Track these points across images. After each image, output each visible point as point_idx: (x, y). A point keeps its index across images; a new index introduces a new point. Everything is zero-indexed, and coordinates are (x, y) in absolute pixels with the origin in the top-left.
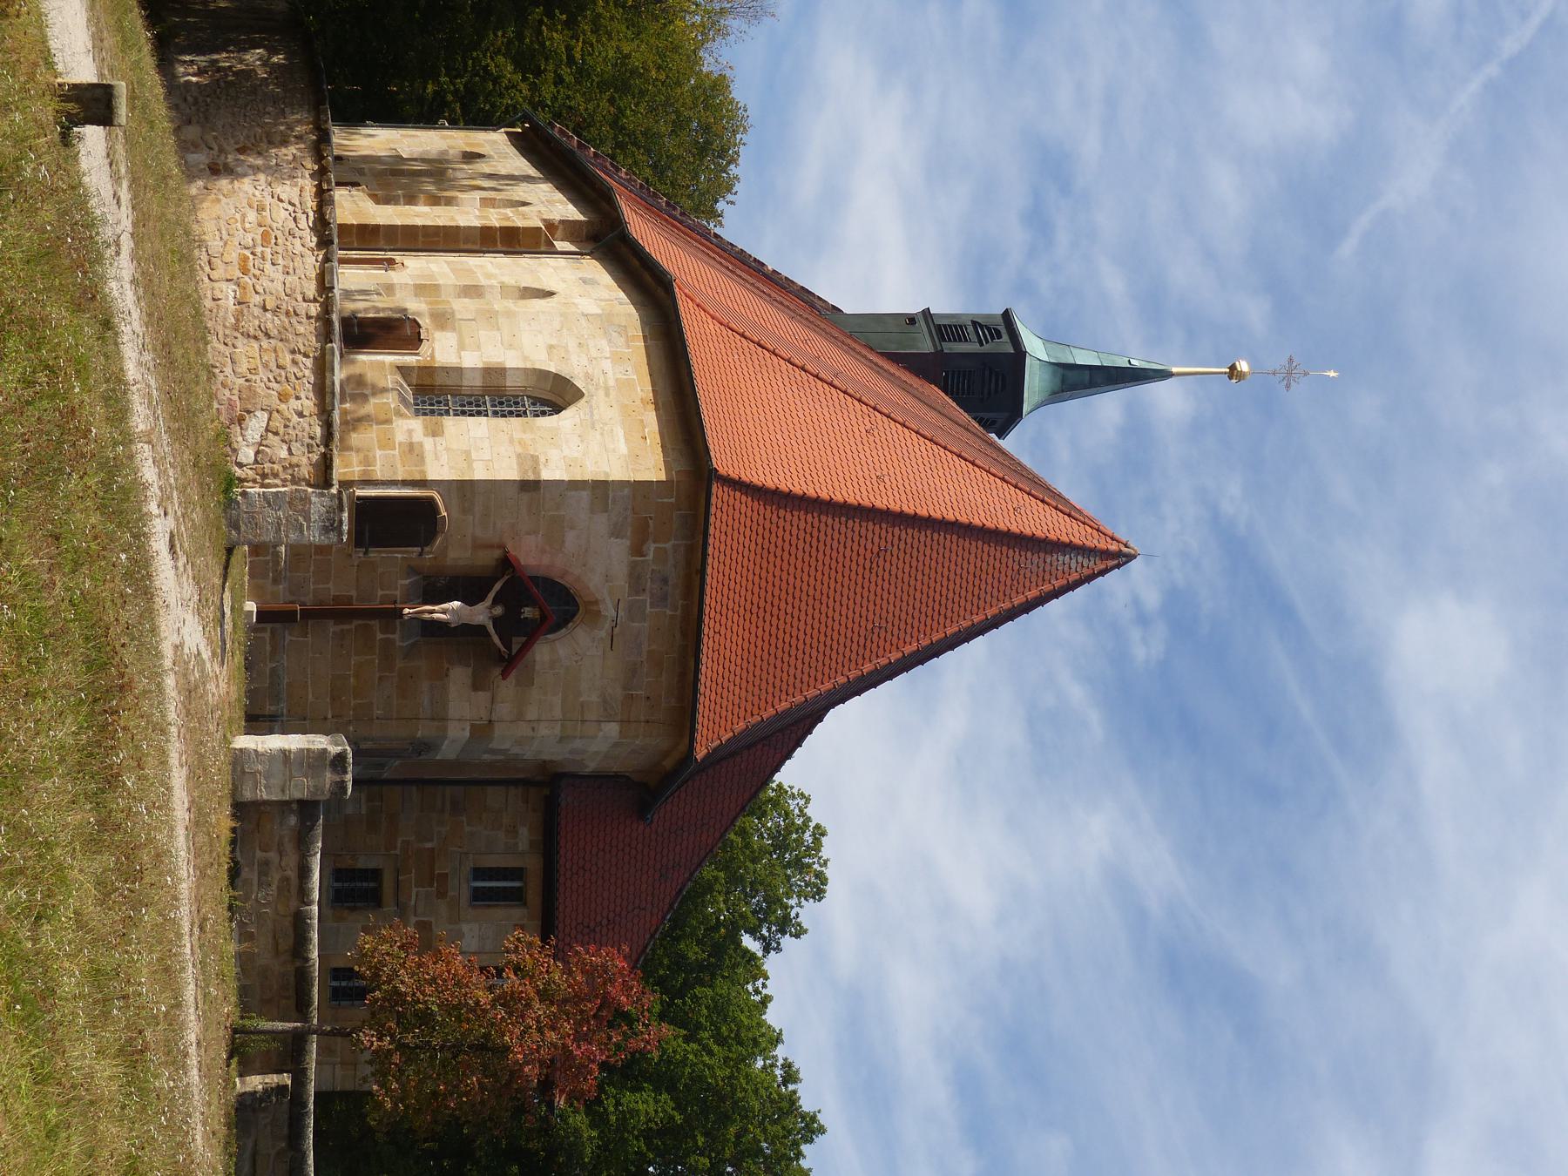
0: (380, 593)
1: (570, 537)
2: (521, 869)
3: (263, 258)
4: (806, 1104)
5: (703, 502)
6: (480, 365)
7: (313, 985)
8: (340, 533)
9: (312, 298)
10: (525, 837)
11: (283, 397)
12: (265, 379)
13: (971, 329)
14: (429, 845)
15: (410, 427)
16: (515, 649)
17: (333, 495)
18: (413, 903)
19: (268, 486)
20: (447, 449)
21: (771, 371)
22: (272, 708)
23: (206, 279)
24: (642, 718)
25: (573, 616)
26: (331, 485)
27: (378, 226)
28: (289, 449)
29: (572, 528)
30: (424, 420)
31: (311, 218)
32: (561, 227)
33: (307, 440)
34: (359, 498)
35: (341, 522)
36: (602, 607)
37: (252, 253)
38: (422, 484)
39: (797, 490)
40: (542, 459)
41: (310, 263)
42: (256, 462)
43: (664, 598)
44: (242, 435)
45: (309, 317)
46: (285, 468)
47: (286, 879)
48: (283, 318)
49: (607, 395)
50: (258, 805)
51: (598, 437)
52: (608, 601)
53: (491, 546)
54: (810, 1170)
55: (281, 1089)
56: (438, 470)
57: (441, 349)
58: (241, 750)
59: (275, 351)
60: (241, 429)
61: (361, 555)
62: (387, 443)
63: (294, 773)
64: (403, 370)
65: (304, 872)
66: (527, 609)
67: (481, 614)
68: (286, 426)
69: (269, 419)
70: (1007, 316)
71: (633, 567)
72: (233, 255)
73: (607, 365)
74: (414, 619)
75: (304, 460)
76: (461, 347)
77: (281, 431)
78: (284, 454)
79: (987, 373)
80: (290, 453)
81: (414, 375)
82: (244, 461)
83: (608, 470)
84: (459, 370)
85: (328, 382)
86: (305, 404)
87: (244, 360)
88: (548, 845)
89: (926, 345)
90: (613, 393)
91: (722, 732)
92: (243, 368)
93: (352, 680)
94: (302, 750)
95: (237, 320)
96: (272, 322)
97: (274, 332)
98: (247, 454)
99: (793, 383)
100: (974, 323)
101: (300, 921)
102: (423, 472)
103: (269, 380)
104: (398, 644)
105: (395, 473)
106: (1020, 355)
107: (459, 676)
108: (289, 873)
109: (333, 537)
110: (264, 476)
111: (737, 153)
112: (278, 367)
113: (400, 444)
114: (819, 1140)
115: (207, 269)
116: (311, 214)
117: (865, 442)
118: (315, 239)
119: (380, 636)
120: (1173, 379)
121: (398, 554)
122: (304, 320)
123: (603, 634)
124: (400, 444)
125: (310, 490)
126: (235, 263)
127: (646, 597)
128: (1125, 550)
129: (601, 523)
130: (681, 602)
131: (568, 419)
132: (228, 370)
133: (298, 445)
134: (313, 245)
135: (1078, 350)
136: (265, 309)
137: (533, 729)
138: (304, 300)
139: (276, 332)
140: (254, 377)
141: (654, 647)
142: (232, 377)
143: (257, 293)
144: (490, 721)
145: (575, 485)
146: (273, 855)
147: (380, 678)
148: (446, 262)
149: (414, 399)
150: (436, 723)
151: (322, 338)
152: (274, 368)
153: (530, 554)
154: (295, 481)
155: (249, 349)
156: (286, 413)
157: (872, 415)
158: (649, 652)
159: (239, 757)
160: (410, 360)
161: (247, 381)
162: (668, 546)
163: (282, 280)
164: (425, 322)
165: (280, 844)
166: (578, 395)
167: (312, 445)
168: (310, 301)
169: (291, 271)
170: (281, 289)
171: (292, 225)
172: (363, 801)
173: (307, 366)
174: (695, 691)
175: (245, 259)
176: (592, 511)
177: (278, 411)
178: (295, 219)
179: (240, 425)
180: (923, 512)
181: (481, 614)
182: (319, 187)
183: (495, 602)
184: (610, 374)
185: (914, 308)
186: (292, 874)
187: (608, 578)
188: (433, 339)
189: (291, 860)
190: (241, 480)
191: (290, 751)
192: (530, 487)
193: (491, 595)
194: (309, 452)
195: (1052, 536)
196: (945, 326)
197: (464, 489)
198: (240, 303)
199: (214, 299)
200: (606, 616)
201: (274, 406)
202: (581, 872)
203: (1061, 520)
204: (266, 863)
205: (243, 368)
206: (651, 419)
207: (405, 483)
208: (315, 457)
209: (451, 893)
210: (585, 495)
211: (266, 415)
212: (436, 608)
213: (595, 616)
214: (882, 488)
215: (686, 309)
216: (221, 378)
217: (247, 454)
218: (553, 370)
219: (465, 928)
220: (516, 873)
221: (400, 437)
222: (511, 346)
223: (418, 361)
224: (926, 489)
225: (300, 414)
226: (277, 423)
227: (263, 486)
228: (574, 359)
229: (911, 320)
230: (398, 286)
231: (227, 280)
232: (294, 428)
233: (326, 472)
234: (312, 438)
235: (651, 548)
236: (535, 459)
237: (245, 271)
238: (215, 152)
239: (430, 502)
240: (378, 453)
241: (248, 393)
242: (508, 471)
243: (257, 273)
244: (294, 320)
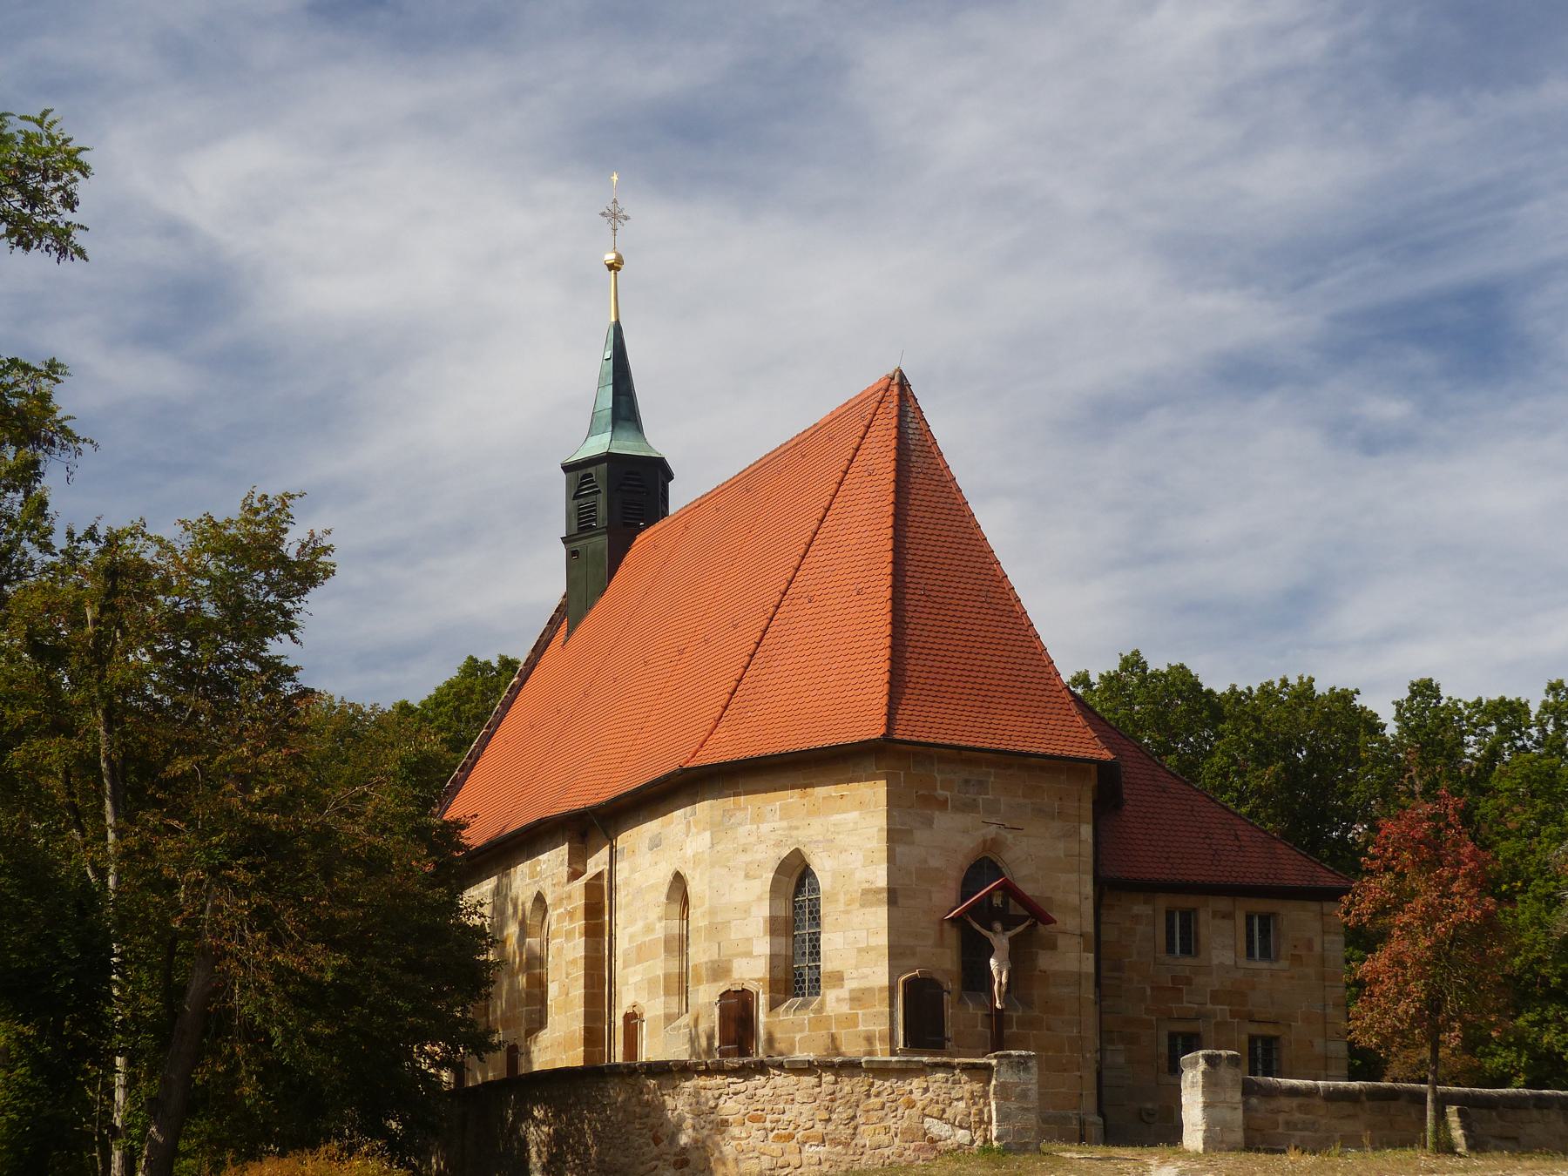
0: (979, 1028)
1: (935, 863)
2: (1167, 912)
3: (778, 1121)
4: (1113, 666)
5: (904, 747)
6: (768, 938)
7: (1379, 1087)
8: (1029, 1056)
9: (817, 1080)
10: (1140, 909)
11: (911, 1105)
12: (894, 1120)
13: (582, 501)
14: (1149, 991)
15: (833, 1000)
16: (1022, 912)
17: (998, 1062)
18: (1196, 1006)
19: (990, 1117)
20: (857, 968)
21: (760, 684)
22: (1074, 1122)
23: (799, 1171)
24: (1076, 804)
25: (991, 861)
26: (990, 1064)
27: (586, 1029)
28: (957, 1100)
29: (926, 861)
30: (826, 987)
31: (735, 1080)
32: (574, 866)
33: (949, 1085)
34: (905, 1045)
35: (1020, 1056)
36: (989, 837)
37: (772, 1131)
38: (892, 989)
39: (886, 666)
40: (866, 886)
41: (781, 1080)
42: (969, 1128)
43: (981, 783)
44: (945, 1140)
45: (836, 1082)
46: (974, 1104)
47: (1300, 1107)
48: (836, 1104)
49: (797, 828)
50: (1248, 1128)
51: (841, 836)
52: (984, 831)
53: (942, 931)
54: (1169, 665)
55: (1461, 1113)
56: (878, 974)
57: (752, 971)
58: (1204, 1144)
59: (868, 1111)
60: (940, 1140)
61: (950, 1044)
62: (851, 1021)
63: (1222, 1099)
64: (773, 1005)
65: (1293, 1092)
66: (994, 902)
67: (1001, 941)
68: (937, 1102)
69: (932, 1117)
70: (567, 468)
71: (956, 809)
72: (776, 1148)
73: (765, 828)
74: (1004, 1001)
75: (967, 1087)
76: (748, 954)
77: (941, 1106)
78: (962, 1105)
79: (624, 488)
80: (961, 1099)
81: (778, 996)
82: (969, 1138)
83: (876, 829)
84: (773, 957)
85: (898, 1066)
86: (916, 1086)
87: (877, 1137)
88: (1149, 888)
89: (601, 542)
90: (795, 823)
91: (1087, 736)
92: (885, 1139)
93: (1050, 1054)
94: (1203, 1092)
95: (839, 1144)
96: (841, 1113)
97: (850, 1112)
98: (962, 1136)
99: (769, 665)
100: (575, 497)
101: (1333, 1096)
102: (881, 989)
103: (895, 1116)
104: (1020, 1013)
105: (882, 1013)
106: (609, 458)
108: (1294, 1105)
109: (1032, 1064)
110: (981, 1121)
111: (352, 705)
112: (883, 1108)
113: (851, 1009)
114: (1145, 656)
115: (787, 1170)
116: (730, 1080)
117: (822, 604)
118: (757, 1077)
119: (1015, 1029)
120: (621, 321)
121: (949, 1012)
122: (839, 1086)
123: (1010, 837)
124: (851, 1009)
125: (994, 1082)
126: (783, 1145)
127: (980, 799)
128: (896, 380)
129: (921, 835)
130: (984, 769)
131: (823, 867)
132: (887, 1152)
133: (953, 1092)
134: (763, 1079)
135: (598, 404)
136: (829, 1120)
137: (1086, 898)
138: (820, 1086)
139: (850, 1110)
140: (893, 1130)
141: (1020, 793)
142: (893, 1150)
143: (813, 1127)
144: (1081, 935)
145: (891, 859)
146: (1281, 1118)
147: (1048, 1030)
148: (624, 968)
149: (797, 996)
150: (1083, 982)
151: (856, 1071)
152: (884, 1112)
153: (945, 899)
154: (985, 1095)
155: (866, 1133)
156: (925, 1102)
157: (791, 597)
158: (1024, 797)
159: (1214, 1142)
160: (763, 1000)
161: (896, 1135)
162: (939, 778)
163: (798, 1105)
164: (723, 986)
165: (1272, 1111)
166: (797, 853)
167: (954, 1080)
168: (821, 1081)
169: (791, 1097)
170: (809, 1106)
171: (742, 1097)
172: (1113, 1048)
173: (883, 1085)
174: (1059, 758)
175: (779, 1138)
176: (913, 843)
177: (924, 1109)
178: (735, 1094)
179: (937, 1141)
180: (889, 556)
181: (1001, 941)
182: (700, 1073)
183: (991, 929)
184: (776, 825)
185: (561, 551)
186: (1295, 1102)
187: (965, 831)
188: (741, 979)
189: (1284, 1102)
190: (985, 1141)
191: (1204, 1102)
192: (893, 896)
193: (985, 932)
194: (960, 1083)
195: (893, 443)
196: (579, 524)
197: (896, 953)
198: (824, 1141)
199: (820, 1164)
200: (997, 833)
201: (920, 1112)
202: (1171, 861)
203: (874, 435)
204: (1287, 1123)
205: (885, 1139)
206: (820, 792)
207: (892, 1005)
208: (964, 1078)
209: (1188, 973)
210: (899, 849)
211: (927, 1119)
212: (997, 980)
213: (994, 844)
214: (869, 591)
215: (707, 758)
216: (893, 1158)
217: (962, 1136)
218: (771, 875)
219: (1215, 962)
220: (1170, 916)
221: (845, 1009)
222: (747, 911)
223: (763, 993)
224: (863, 552)
225: (926, 1090)
226: (935, 1109)
227: (990, 1123)
228: (759, 856)
229: (572, 555)
230: (667, 1011)
231: (800, 1152)
232: (938, 1095)
233: (978, 1069)
234: (947, 1081)
235: (941, 793)
236: (865, 892)
237: (791, 1137)
238: (660, 1164)
239: (905, 982)
240: (861, 1028)
241: (909, 1135)
242: (879, 916)
243: (792, 1125)
244: (839, 1095)
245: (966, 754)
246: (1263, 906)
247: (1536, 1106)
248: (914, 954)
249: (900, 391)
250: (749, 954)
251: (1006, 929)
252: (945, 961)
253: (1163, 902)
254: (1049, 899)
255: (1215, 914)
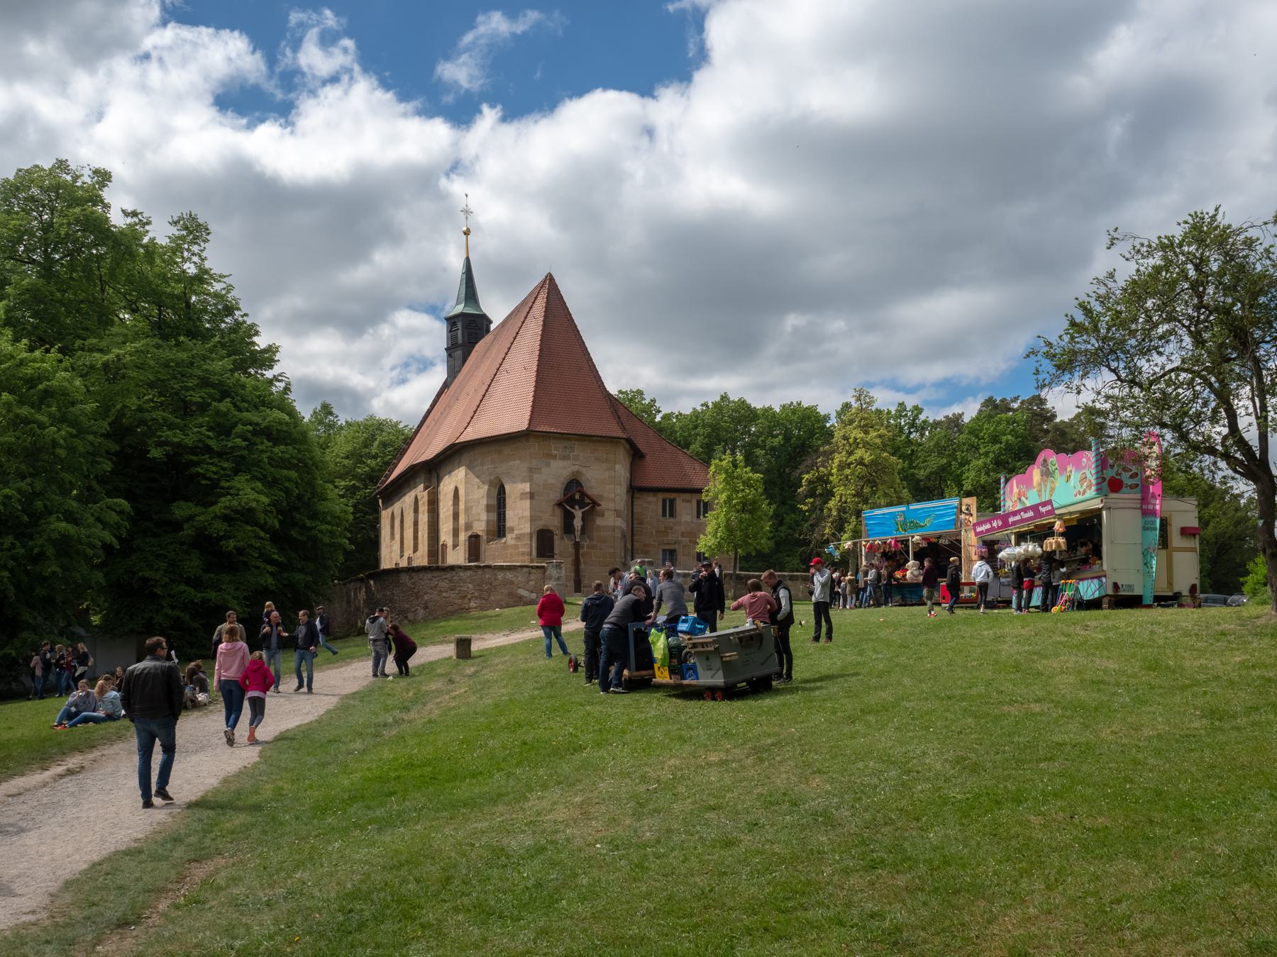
1: (549, 481)
15: (509, 539)
56: (526, 528)
57: (480, 527)
71: (560, 459)
73: (485, 468)
84: (488, 522)
88: (655, 490)
89: (459, 353)
100: (450, 331)
107: (599, 521)
164: (470, 533)
183: (574, 508)
207: (531, 540)
219: (683, 520)
220: (664, 501)
221: (513, 542)
235: (554, 452)
236: (522, 494)
245: (565, 436)
246: (672, 496)
247: (790, 579)
248: (541, 519)
249: (550, 284)
250: (479, 520)
251: (580, 508)
252: (553, 521)
253: (661, 496)
254: (601, 496)
255: (683, 501)
